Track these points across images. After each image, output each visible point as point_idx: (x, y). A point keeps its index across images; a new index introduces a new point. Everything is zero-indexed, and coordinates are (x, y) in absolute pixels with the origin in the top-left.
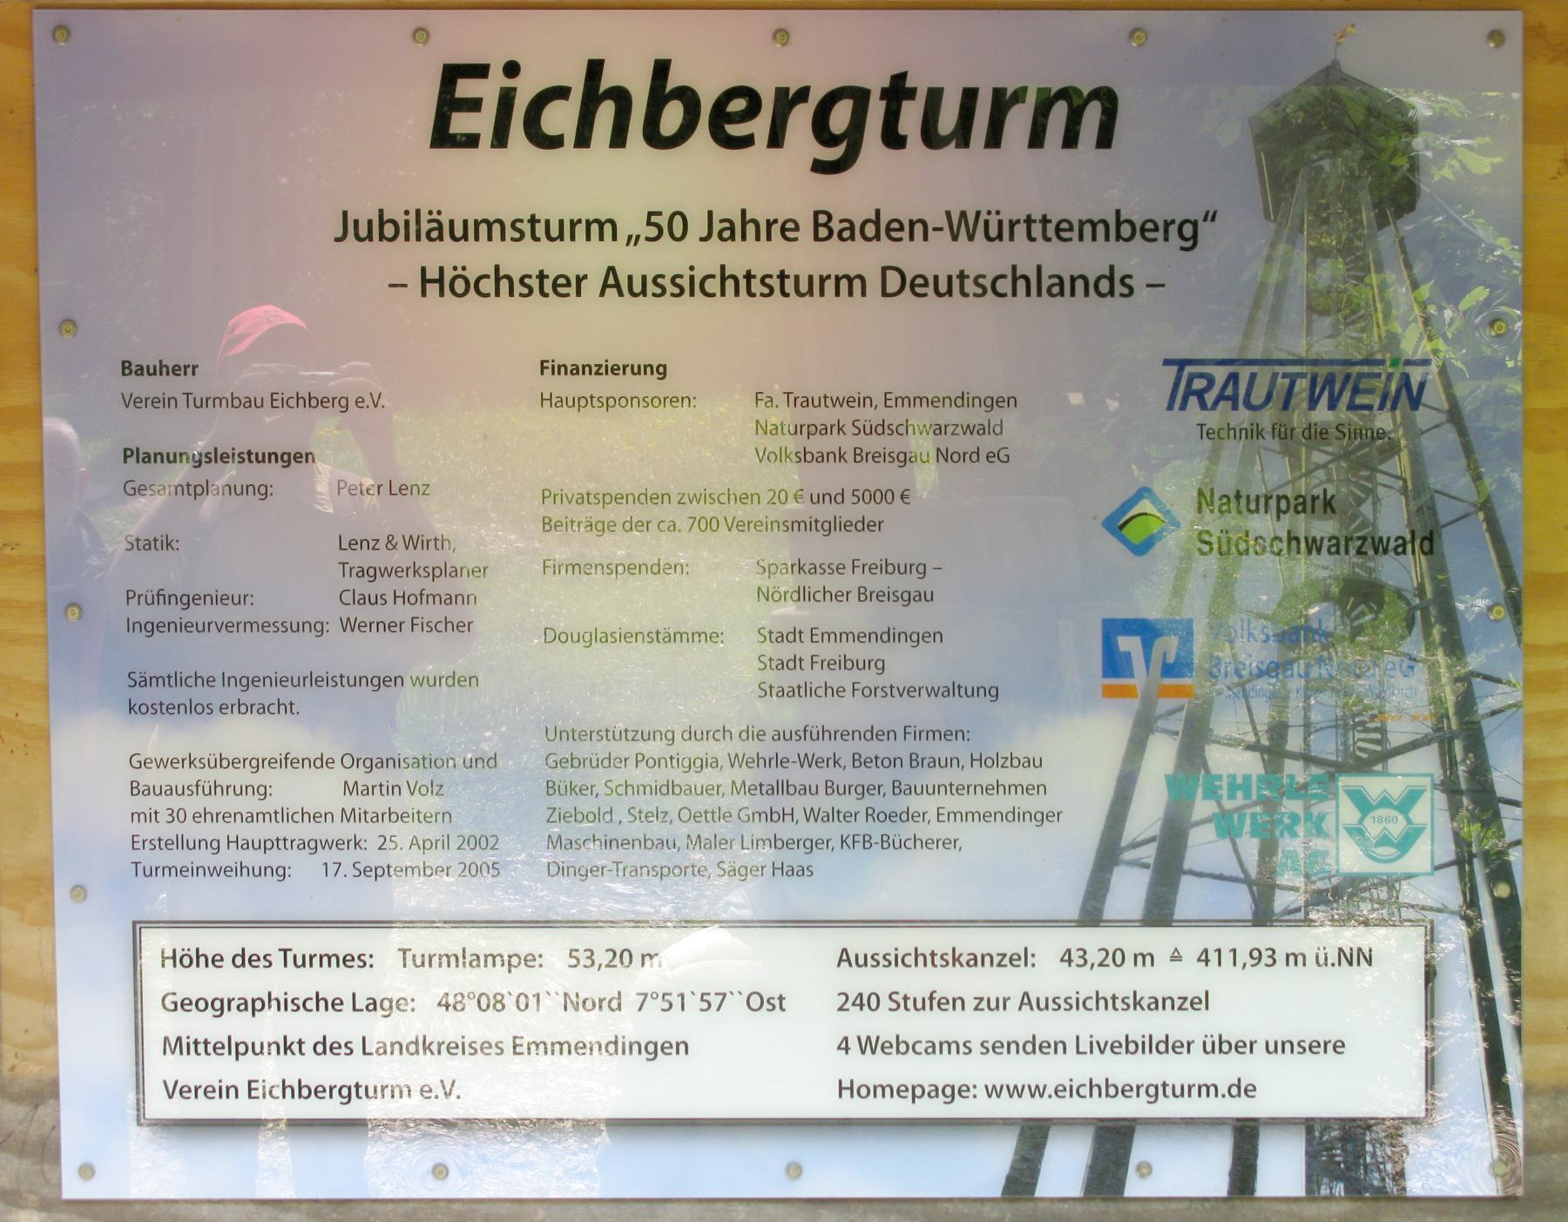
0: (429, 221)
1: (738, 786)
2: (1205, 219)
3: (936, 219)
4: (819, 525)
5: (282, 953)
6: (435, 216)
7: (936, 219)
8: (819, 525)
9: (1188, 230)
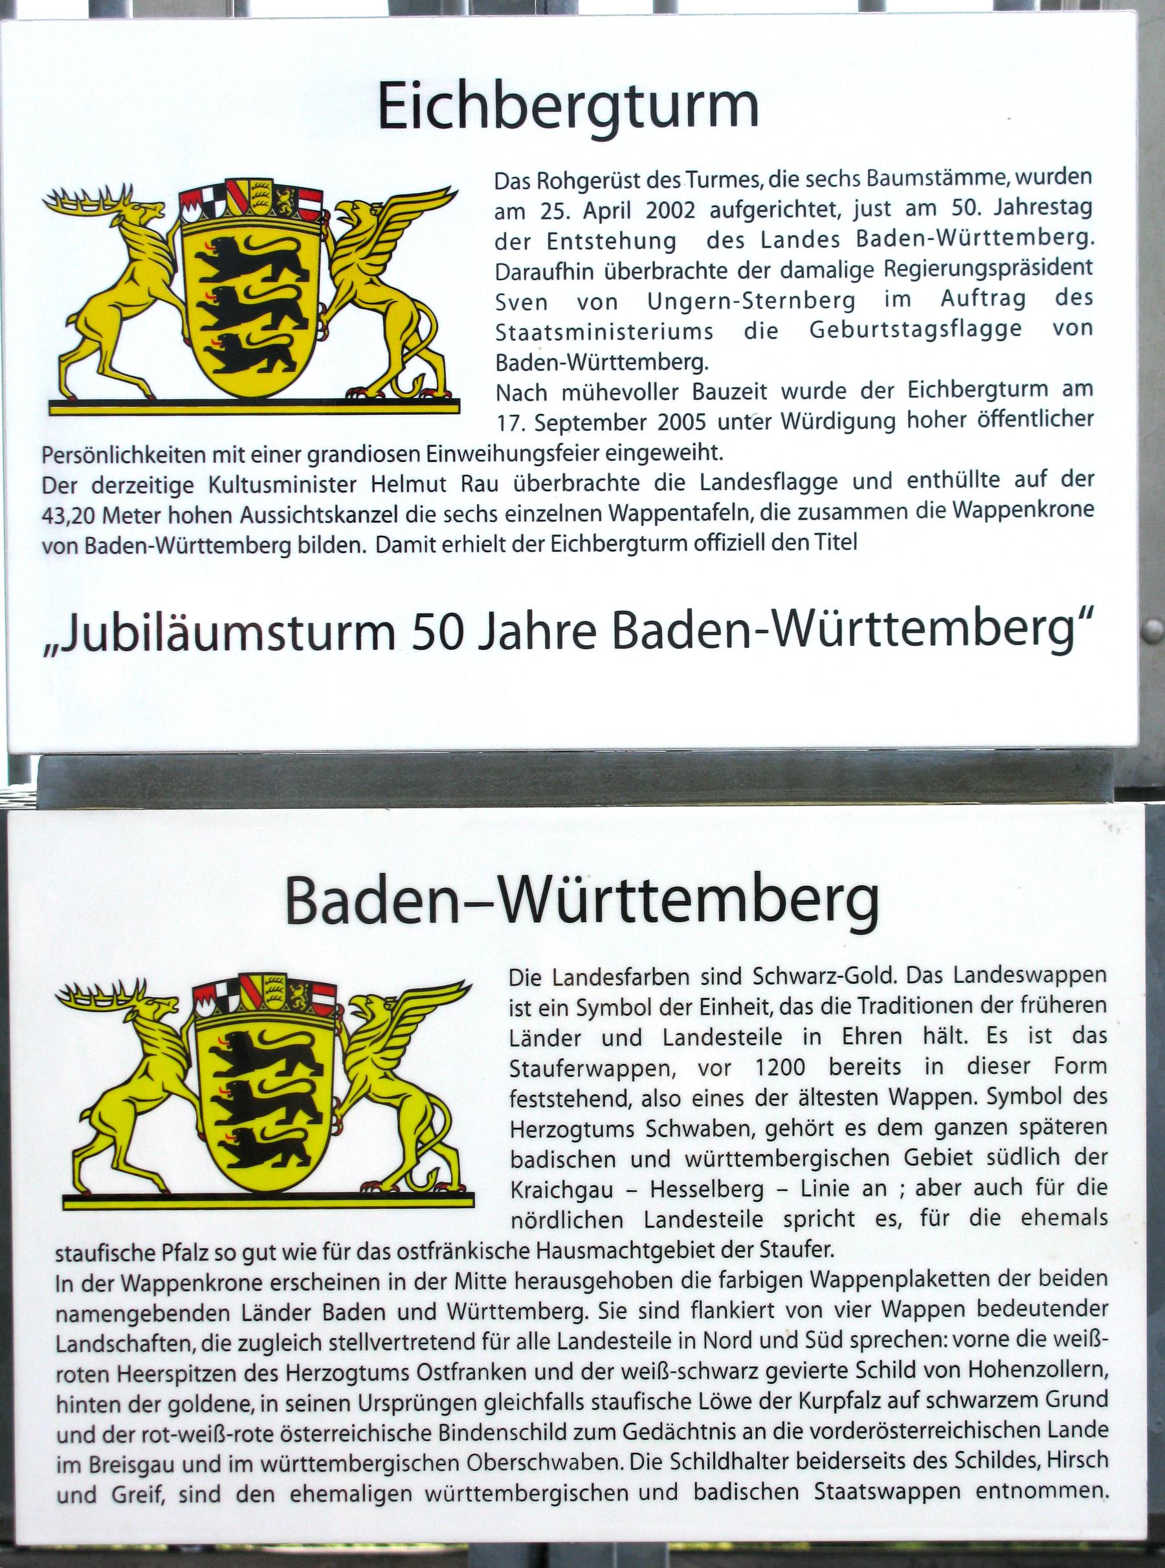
0: (172, 626)
2: (1081, 616)
3: (760, 619)
4: (649, 1251)
6: (178, 620)
7: (760, 619)
8: (649, 1251)
9: (1061, 631)
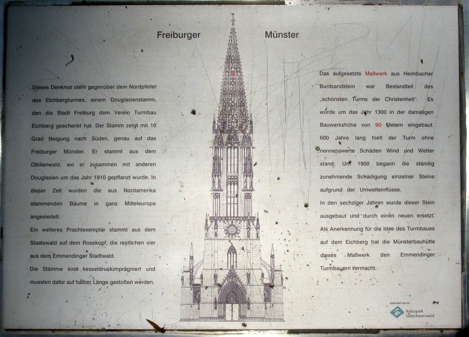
1: (66, 151)
5: (404, 137)
